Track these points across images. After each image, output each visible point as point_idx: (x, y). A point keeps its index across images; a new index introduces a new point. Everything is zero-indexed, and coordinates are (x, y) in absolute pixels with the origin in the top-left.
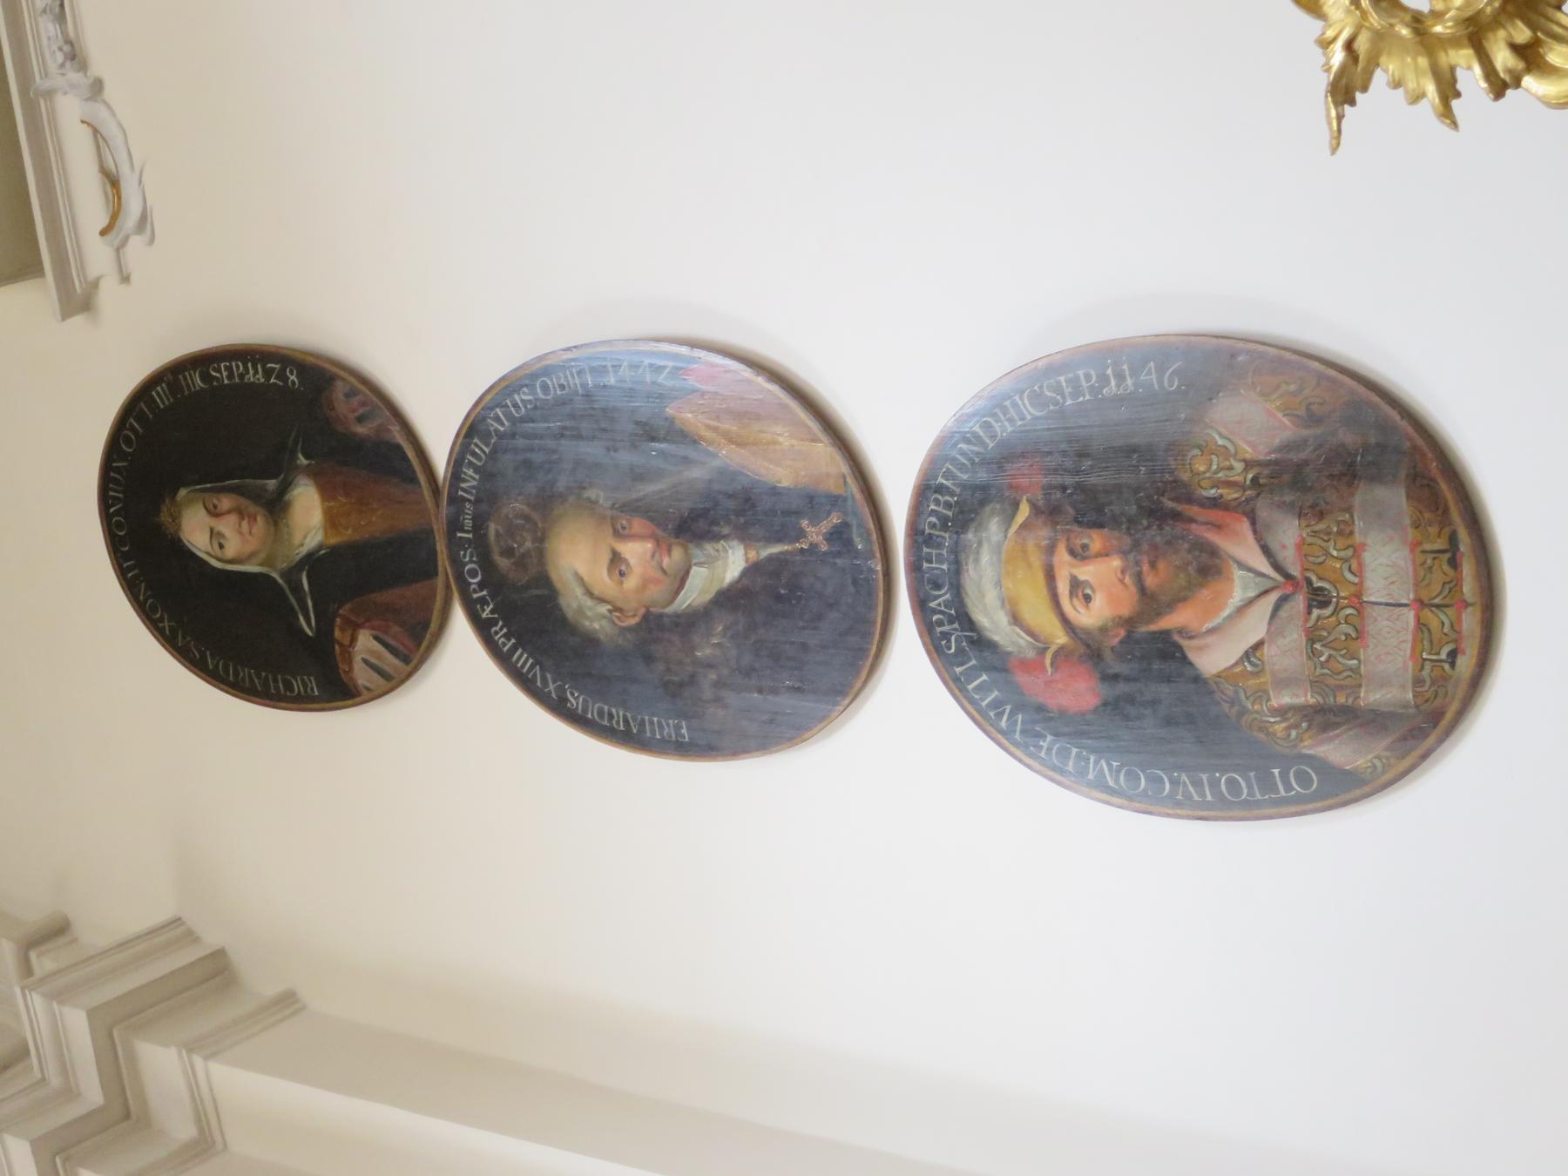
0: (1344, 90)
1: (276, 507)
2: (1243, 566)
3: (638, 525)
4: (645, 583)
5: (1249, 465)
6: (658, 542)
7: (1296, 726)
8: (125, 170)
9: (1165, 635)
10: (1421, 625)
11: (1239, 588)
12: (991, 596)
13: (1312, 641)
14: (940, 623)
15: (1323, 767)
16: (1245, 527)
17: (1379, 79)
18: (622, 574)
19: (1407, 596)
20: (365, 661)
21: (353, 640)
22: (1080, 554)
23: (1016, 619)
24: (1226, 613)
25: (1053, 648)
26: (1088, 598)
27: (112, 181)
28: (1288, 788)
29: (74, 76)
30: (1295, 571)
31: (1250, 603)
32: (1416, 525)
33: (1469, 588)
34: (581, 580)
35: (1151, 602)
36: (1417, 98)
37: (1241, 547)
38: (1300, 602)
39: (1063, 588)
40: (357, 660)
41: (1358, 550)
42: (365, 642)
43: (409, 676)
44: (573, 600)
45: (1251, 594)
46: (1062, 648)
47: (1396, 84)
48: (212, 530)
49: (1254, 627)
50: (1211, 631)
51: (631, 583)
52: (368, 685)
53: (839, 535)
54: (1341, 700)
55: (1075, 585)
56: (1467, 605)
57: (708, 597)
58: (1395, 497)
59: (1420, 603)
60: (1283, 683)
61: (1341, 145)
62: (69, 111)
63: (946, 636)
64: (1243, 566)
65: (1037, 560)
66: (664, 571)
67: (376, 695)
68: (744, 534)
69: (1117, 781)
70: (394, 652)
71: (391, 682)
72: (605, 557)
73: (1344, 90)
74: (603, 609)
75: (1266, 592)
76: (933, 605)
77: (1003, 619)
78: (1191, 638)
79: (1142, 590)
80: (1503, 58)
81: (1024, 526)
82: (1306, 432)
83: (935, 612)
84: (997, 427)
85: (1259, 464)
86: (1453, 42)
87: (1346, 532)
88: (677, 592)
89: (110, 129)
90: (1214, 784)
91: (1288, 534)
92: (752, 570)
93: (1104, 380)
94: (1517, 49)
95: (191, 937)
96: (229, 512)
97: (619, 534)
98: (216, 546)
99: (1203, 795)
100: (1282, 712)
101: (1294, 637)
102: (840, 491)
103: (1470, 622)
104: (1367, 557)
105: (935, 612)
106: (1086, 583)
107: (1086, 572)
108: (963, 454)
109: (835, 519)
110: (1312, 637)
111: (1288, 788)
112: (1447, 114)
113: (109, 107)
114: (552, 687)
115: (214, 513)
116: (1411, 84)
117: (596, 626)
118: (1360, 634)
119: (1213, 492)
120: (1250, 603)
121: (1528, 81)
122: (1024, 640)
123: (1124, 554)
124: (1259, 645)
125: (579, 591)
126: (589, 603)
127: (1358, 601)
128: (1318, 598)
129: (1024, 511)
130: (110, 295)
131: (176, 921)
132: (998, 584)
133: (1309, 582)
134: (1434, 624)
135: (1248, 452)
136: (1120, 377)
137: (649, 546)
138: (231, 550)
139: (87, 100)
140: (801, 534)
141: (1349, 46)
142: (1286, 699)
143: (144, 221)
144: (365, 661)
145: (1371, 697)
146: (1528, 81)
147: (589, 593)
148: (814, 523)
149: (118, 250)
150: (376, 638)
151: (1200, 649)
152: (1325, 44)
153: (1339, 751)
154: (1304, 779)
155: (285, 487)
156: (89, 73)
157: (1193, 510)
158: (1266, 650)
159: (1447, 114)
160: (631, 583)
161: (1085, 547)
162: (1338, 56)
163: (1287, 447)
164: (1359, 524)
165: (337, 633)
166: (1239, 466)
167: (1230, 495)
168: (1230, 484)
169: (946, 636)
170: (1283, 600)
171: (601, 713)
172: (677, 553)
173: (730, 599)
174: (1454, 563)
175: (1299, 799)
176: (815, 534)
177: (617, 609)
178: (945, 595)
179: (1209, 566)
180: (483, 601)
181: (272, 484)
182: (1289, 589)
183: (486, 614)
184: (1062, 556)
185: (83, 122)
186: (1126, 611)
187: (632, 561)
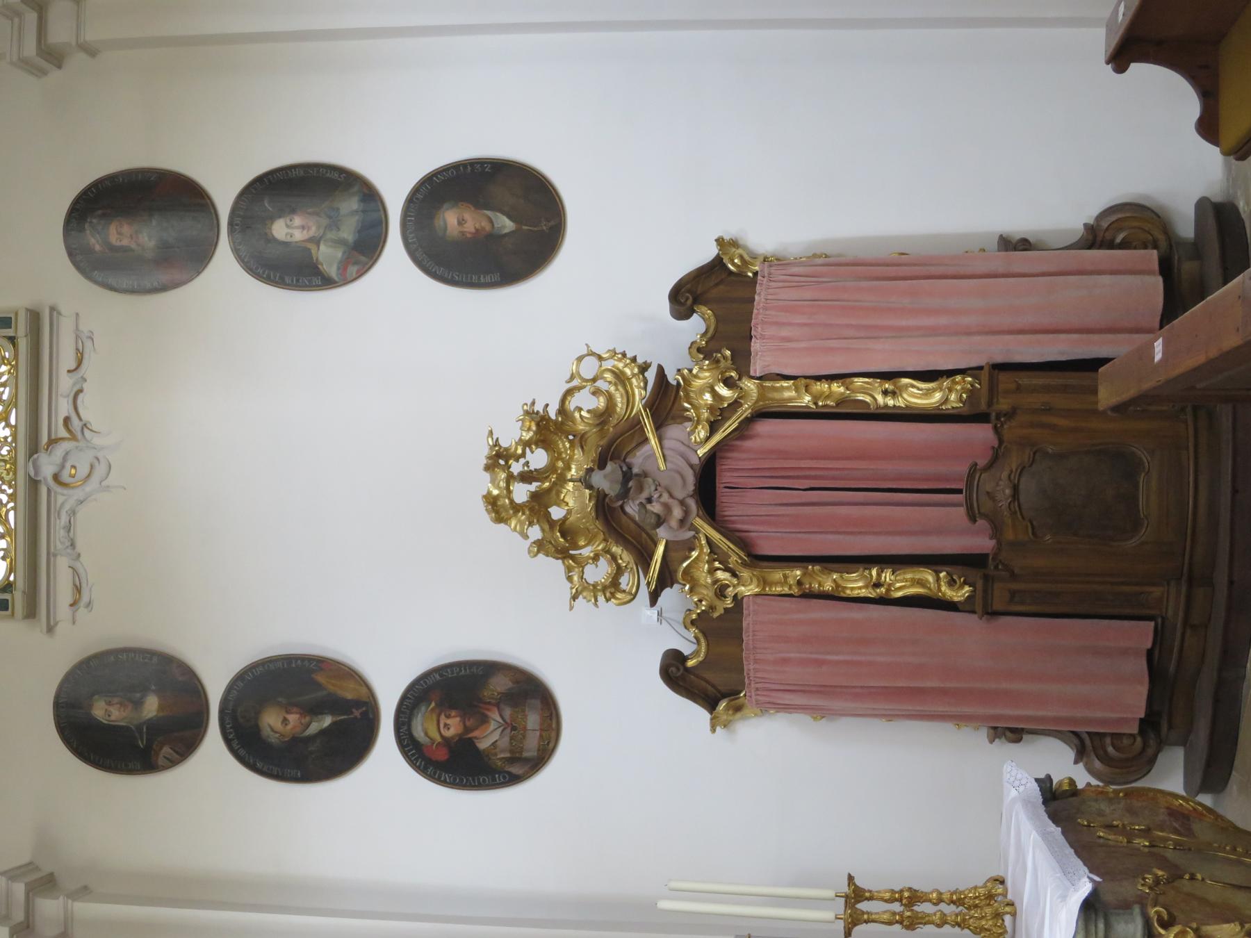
0: (574, 598)
1: (138, 704)
2: (495, 720)
3: (295, 709)
4: (294, 727)
5: (499, 694)
6: (301, 714)
7: (504, 763)
8: (84, 585)
9: (470, 739)
10: (541, 736)
11: (493, 725)
12: (420, 728)
13: (511, 740)
14: (403, 736)
15: (509, 773)
16: (496, 709)
17: (581, 596)
18: (286, 724)
19: (538, 728)
20: (165, 757)
21: (161, 749)
22: (448, 717)
23: (426, 734)
24: (488, 732)
25: (437, 742)
26: (449, 729)
27: (78, 589)
28: (500, 780)
29: (69, 551)
30: (508, 721)
31: (496, 729)
32: (542, 709)
33: (554, 726)
34: (270, 726)
35: (467, 730)
36: (590, 601)
37: (495, 715)
38: (509, 730)
39: (442, 726)
40: (161, 756)
41: (526, 716)
42: (166, 750)
43: (182, 761)
44: (266, 732)
45: (496, 727)
46: (439, 743)
47: (585, 598)
48: (106, 710)
49: (496, 736)
50: (483, 738)
51: (289, 727)
52: (163, 765)
53: (365, 714)
54: (517, 755)
55: (446, 725)
56: (553, 730)
57: (317, 731)
58: (537, 703)
59: (542, 730)
60: (502, 751)
61: (636, 599)
62: (62, 564)
63: (404, 739)
64: (495, 720)
65: (435, 717)
66: (302, 724)
67: (165, 768)
68: (333, 714)
69: (450, 780)
70: (177, 752)
71: (173, 763)
72: (280, 720)
73: (574, 598)
74: (277, 735)
75: (500, 727)
76: (401, 730)
77: (422, 734)
78: (478, 739)
79: (465, 725)
80: (608, 595)
81: (432, 710)
82: (515, 686)
83: (402, 732)
84: (428, 682)
85: (501, 693)
86: (599, 590)
87: (523, 711)
88: (305, 730)
89: (81, 571)
90: (479, 779)
91: (508, 712)
92: (333, 724)
93: (461, 670)
94: (611, 593)
95: (37, 869)
96: (117, 703)
97: (288, 712)
98: (107, 716)
99: (475, 783)
100: (501, 759)
101: (506, 739)
102: (368, 700)
103: (553, 735)
104: (528, 718)
105: (402, 732)
106: (449, 725)
107: (449, 721)
108: (417, 689)
109: (364, 709)
110: (512, 738)
111: (500, 780)
112: (596, 605)
113: (81, 563)
114: (251, 761)
115: (109, 704)
116: (588, 598)
117: (273, 741)
118: (524, 737)
119: (488, 700)
120: (496, 729)
121: (612, 600)
122: (428, 740)
123: (461, 717)
124: (496, 741)
125: (269, 729)
126: (272, 733)
127: (525, 729)
128: (514, 728)
129: (433, 705)
130: (63, 628)
131: (30, 863)
132: (422, 725)
133: (512, 724)
134: (544, 734)
135: (499, 690)
136: (465, 670)
137: (298, 716)
138: (113, 718)
139: (73, 560)
140: (352, 713)
141: (577, 589)
142: (502, 756)
143: (89, 604)
144: (165, 757)
145: (525, 754)
146: (612, 600)
147: (273, 730)
148: (357, 710)
149: (74, 612)
150: (171, 748)
151: (480, 742)
152: (572, 588)
153: (515, 770)
154: (504, 777)
155: (143, 697)
156: (76, 550)
157: (481, 705)
158: (498, 743)
159: (596, 605)
160: (289, 727)
161: (450, 715)
162: (574, 591)
163: (509, 689)
164: (527, 709)
165: (154, 747)
166: (496, 694)
167: (493, 701)
168: (493, 698)
169: (404, 739)
170: (503, 731)
171: (268, 769)
172: (308, 719)
173: (323, 732)
174: (551, 719)
175: (502, 783)
176: (357, 713)
177: (281, 735)
178: (406, 728)
179: (484, 720)
180: (231, 733)
181: (138, 695)
182: (506, 726)
183: (231, 736)
184: (443, 717)
185: (70, 567)
186: (459, 732)
187: (291, 721)
